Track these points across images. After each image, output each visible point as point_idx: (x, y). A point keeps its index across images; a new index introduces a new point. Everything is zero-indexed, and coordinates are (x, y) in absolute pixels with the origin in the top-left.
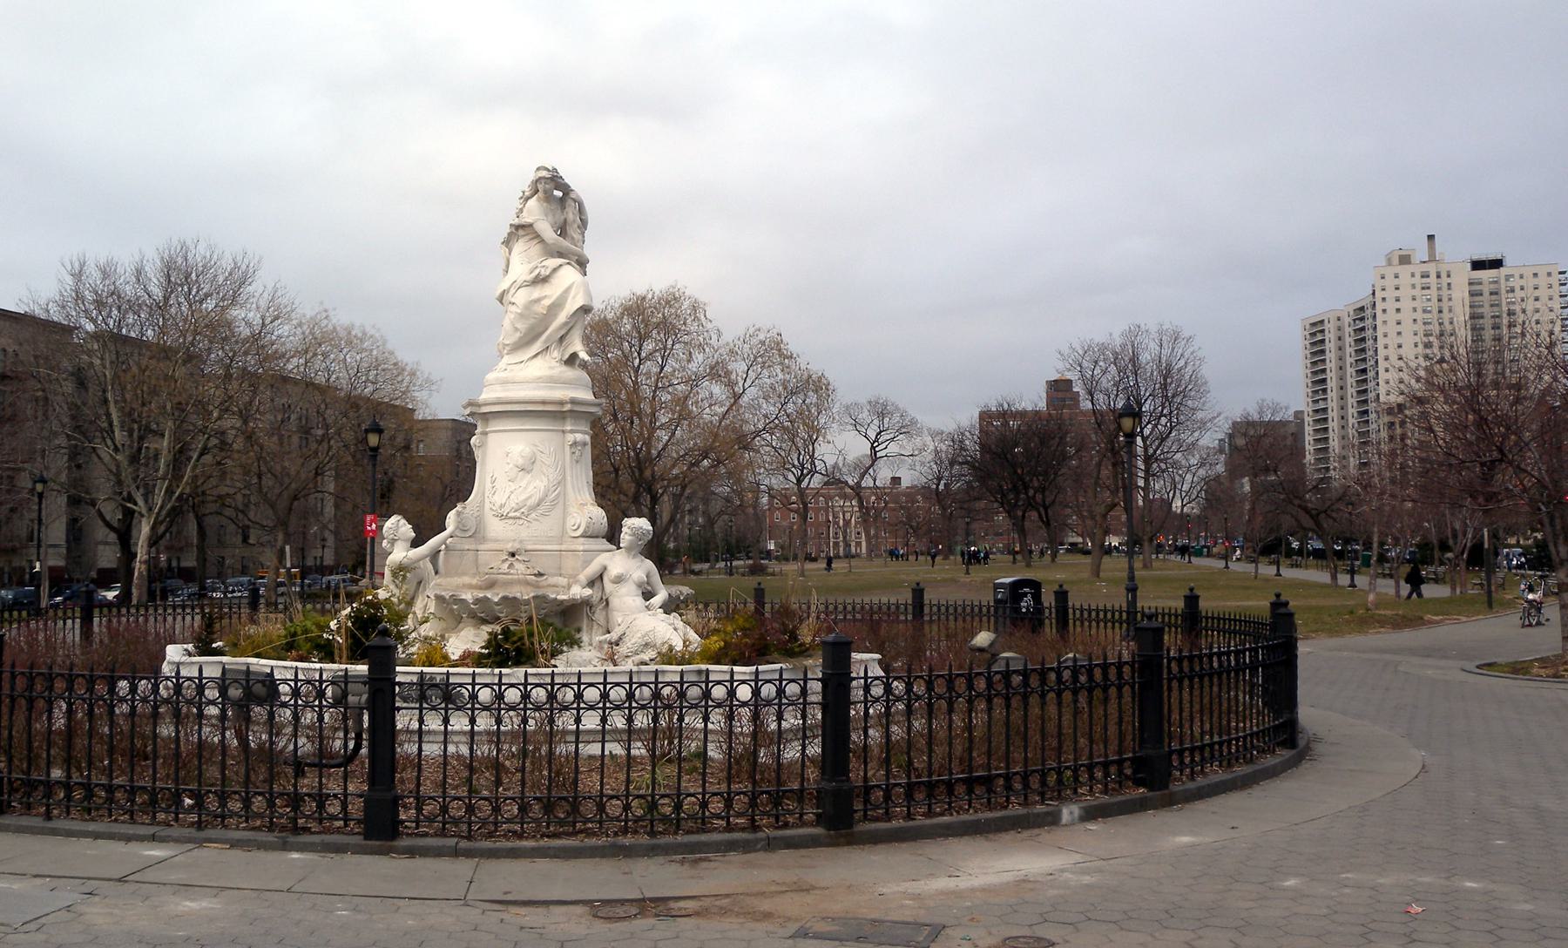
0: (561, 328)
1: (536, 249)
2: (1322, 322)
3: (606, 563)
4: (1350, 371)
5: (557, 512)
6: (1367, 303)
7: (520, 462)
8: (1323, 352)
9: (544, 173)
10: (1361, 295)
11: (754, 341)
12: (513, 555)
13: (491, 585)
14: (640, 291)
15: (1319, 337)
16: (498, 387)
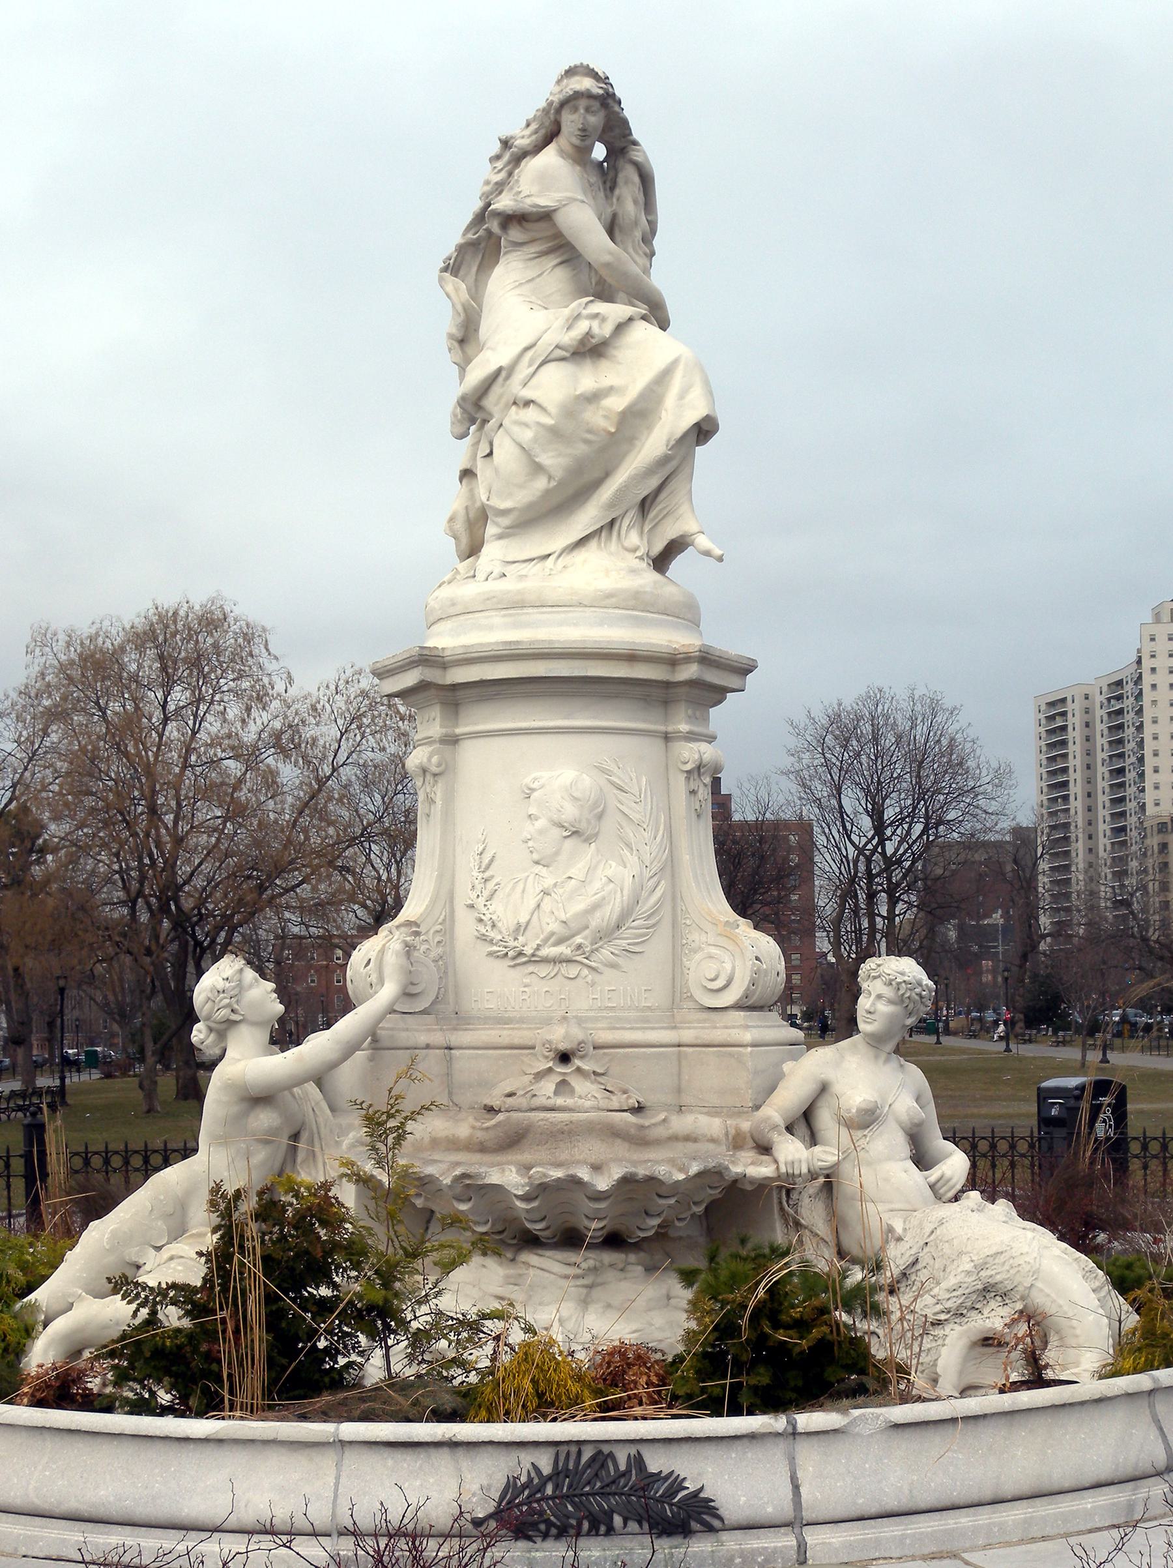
0: (650, 471)
1: (555, 278)
2: (1063, 700)
3: (829, 1074)
4: (1102, 770)
5: (658, 948)
6: (1127, 674)
7: (570, 812)
8: (1064, 743)
9: (586, 84)
10: (1118, 662)
11: (353, 691)
12: (565, 1058)
13: (512, 1140)
14: (169, 600)
15: (1059, 722)
16: (497, 619)
